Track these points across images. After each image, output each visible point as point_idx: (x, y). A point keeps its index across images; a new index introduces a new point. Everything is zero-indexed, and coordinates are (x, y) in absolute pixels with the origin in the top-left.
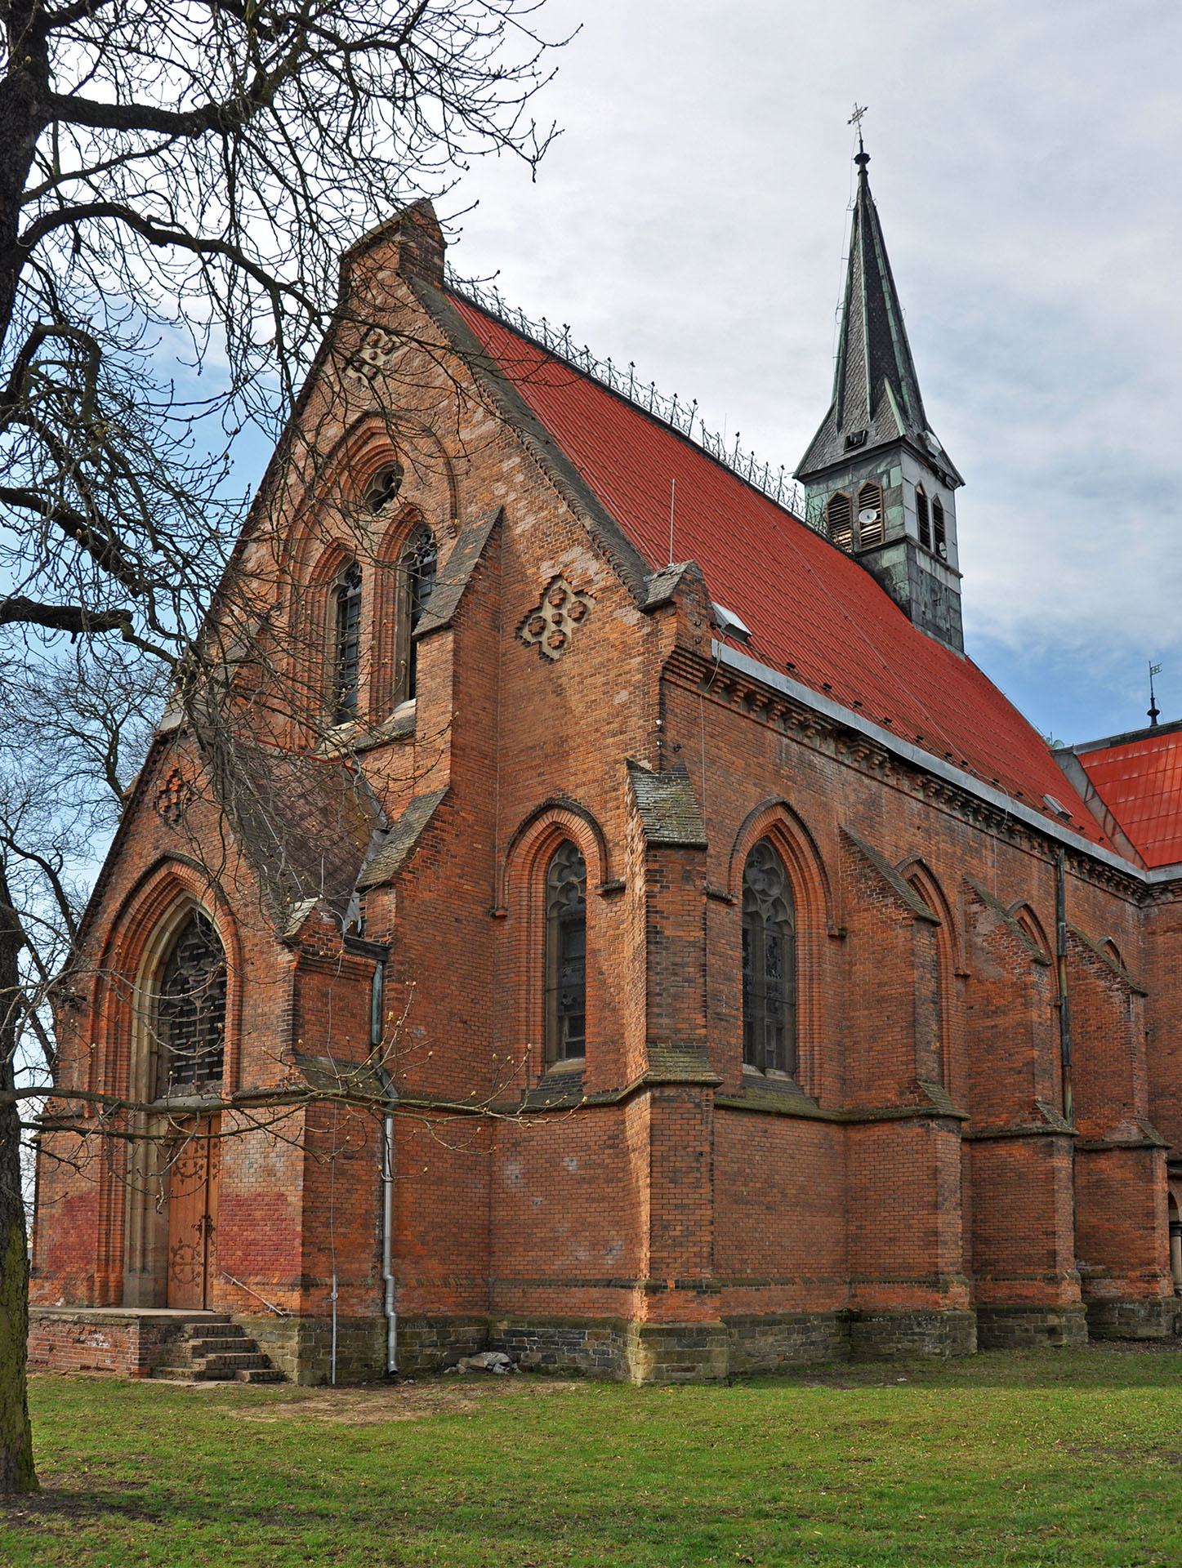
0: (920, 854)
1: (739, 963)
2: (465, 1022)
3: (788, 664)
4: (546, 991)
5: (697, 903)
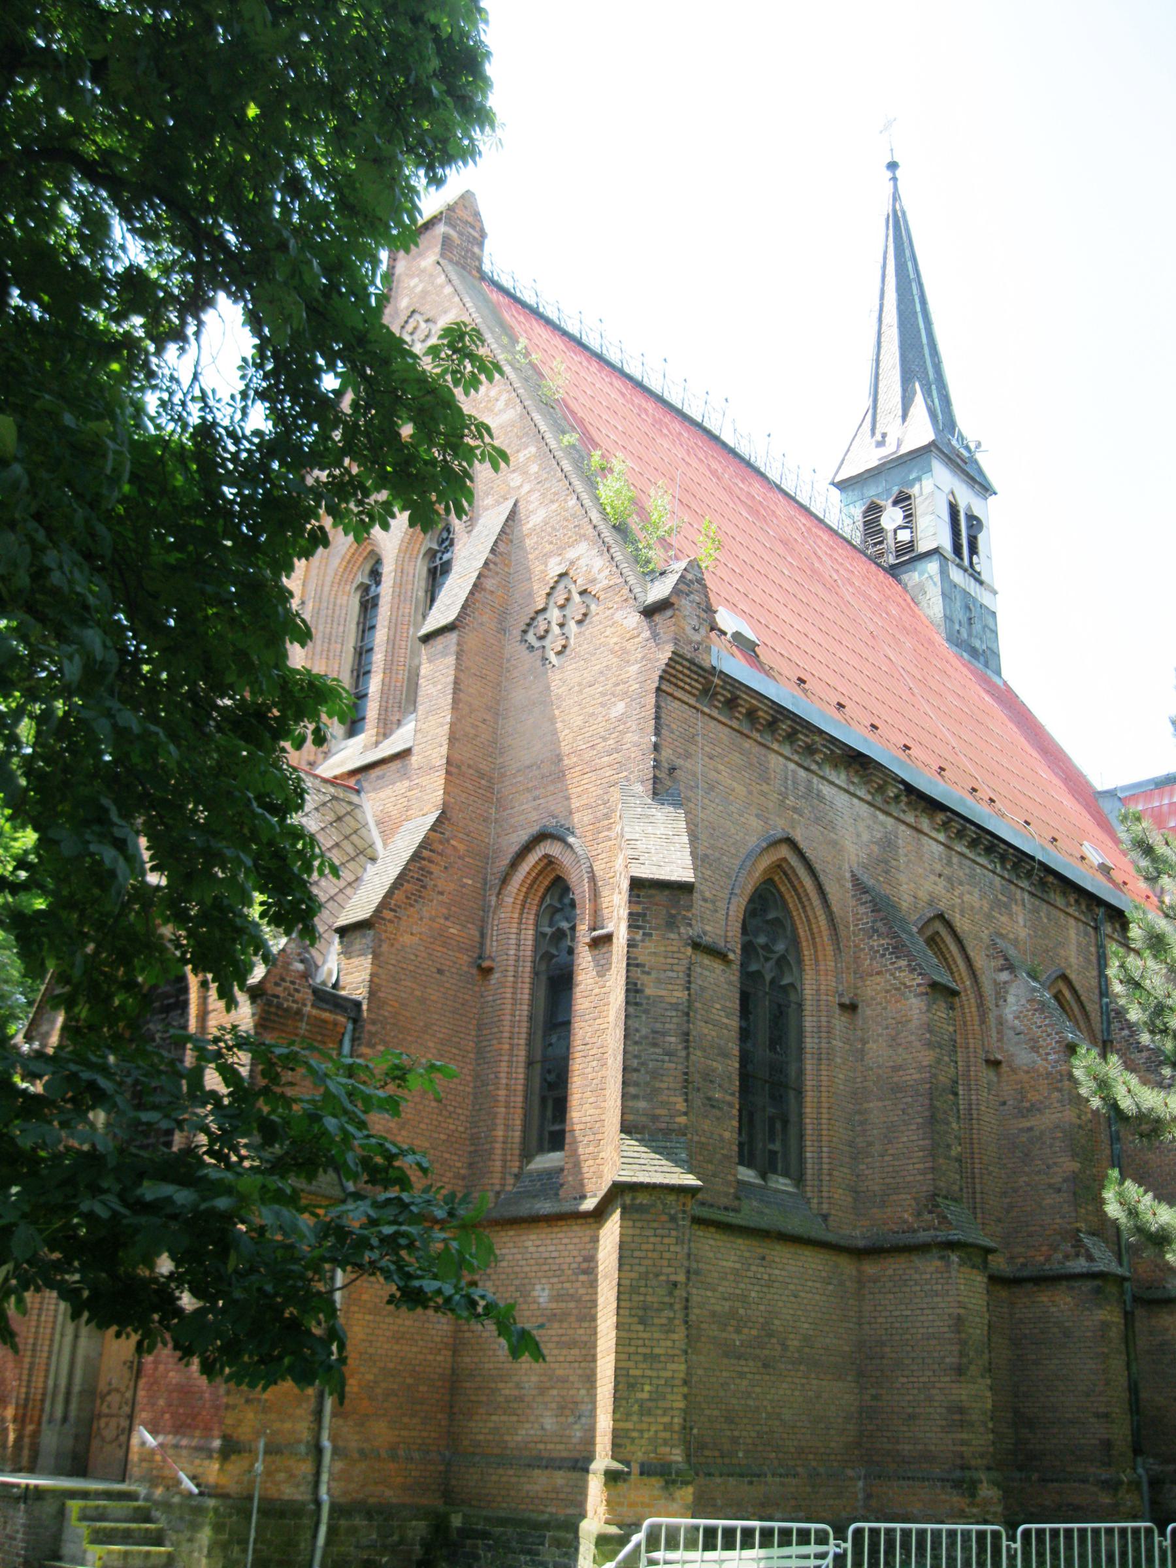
0: (942, 906)
1: (734, 1035)
2: (439, 1101)
3: (799, 679)
4: (530, 1064)
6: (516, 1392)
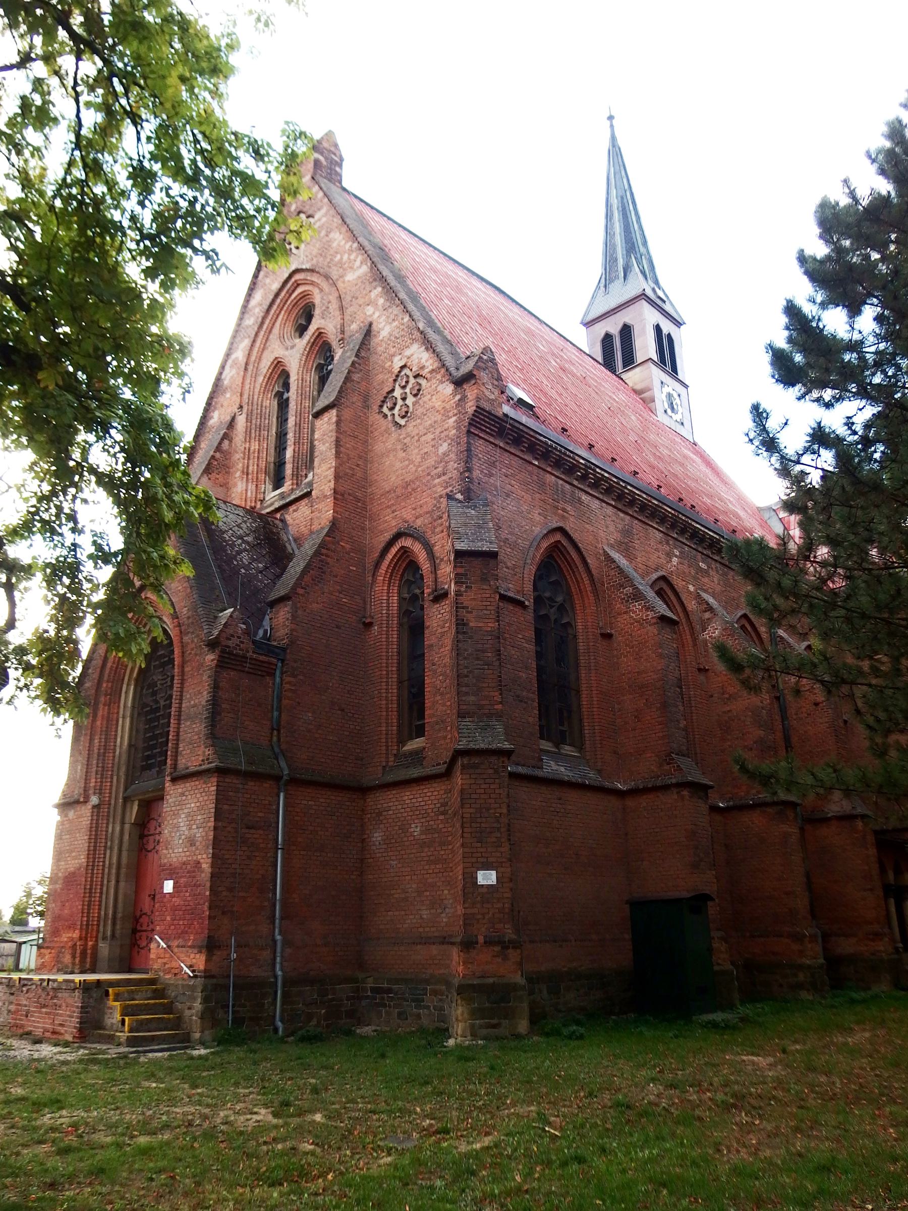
1: (533, 654)
2: (343, 710)
4: (400, 682)
5: (492, 600)
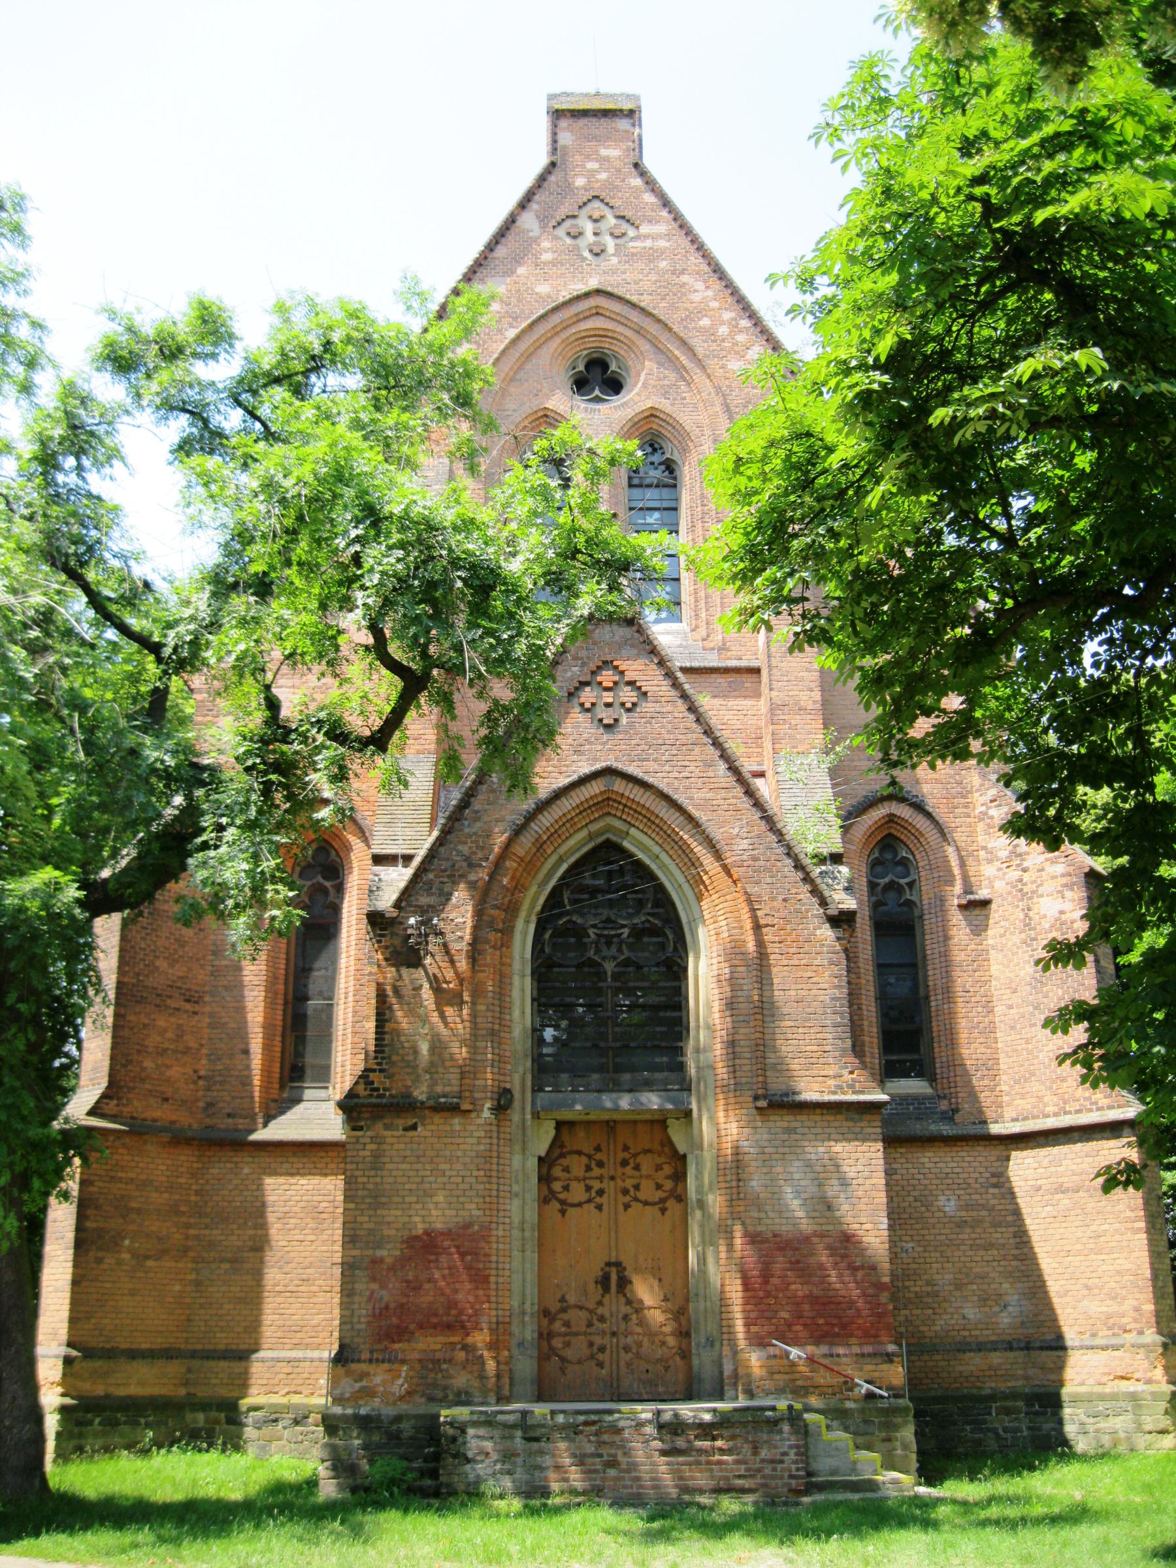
6: (929, 1289)
